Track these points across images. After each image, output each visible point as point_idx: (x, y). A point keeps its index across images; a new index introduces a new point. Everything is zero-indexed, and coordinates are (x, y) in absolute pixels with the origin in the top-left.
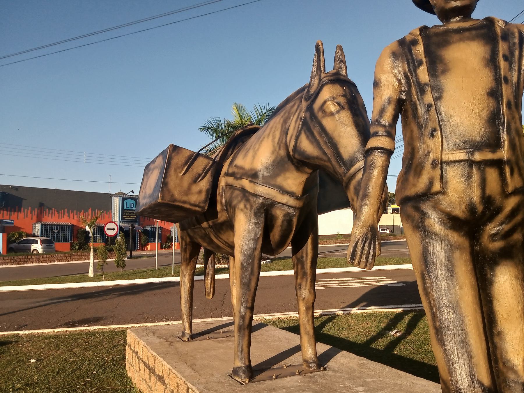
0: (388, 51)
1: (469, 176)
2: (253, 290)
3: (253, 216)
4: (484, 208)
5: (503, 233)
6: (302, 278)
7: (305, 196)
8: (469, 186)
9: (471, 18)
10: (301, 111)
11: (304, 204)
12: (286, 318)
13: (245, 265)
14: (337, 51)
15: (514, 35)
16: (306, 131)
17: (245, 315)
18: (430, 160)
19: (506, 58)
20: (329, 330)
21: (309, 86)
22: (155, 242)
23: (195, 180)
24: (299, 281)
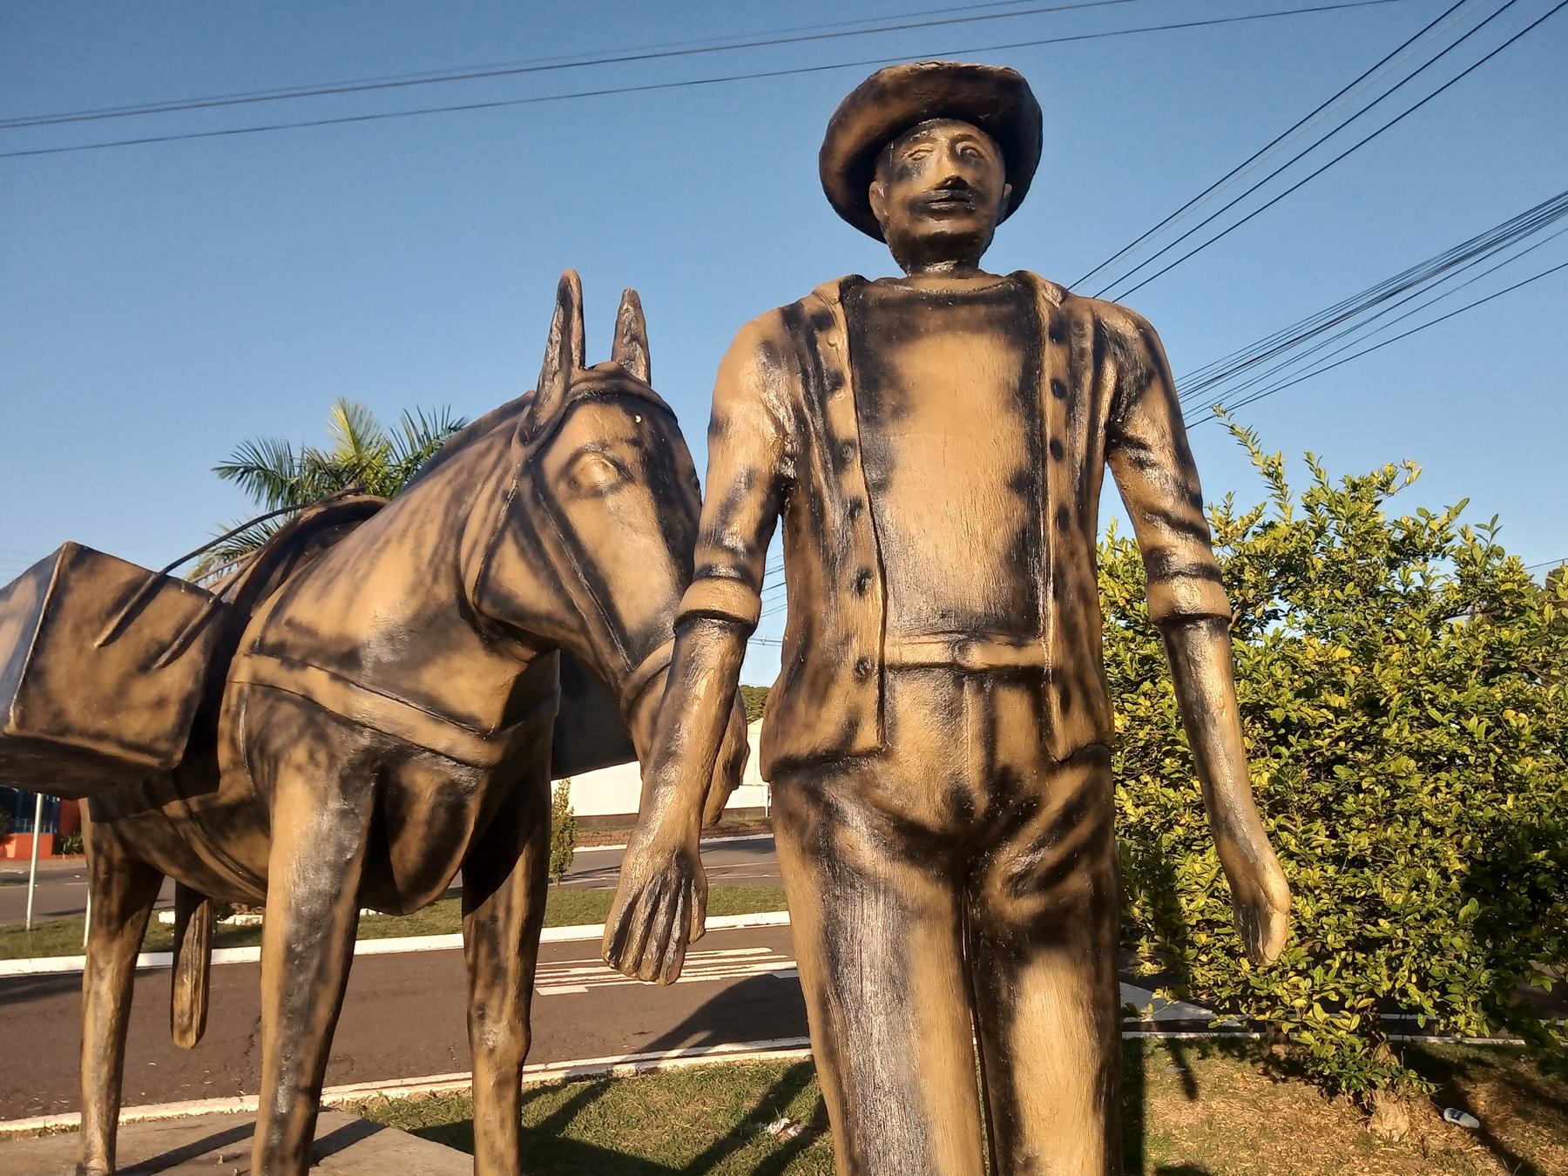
0: (753, 338)
1: (953, 711)
2: (320, 1030)
3: (335, 790)
4: (993, 801)
5: (1040, 871)
6: (490, 986)
7: (510, 730)
8: (954, 737)
9: (980, 267)
10: (506, 472)
11: (506, 753)
12: (457, 1093)
13: (300, 948)
14: (625, 307)
15: (1083, 329)
16: (520, 533)
17: (288, 1113)
18: (851, 657)
19: (1059, 389)
20: (585, 1128)
21: (534, 401)
22: (30, 829)
23: (145, 666)
24: (479, 994)
